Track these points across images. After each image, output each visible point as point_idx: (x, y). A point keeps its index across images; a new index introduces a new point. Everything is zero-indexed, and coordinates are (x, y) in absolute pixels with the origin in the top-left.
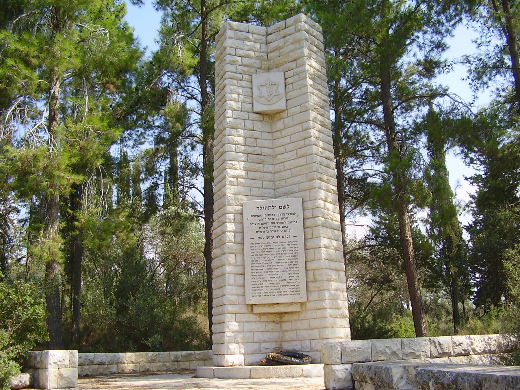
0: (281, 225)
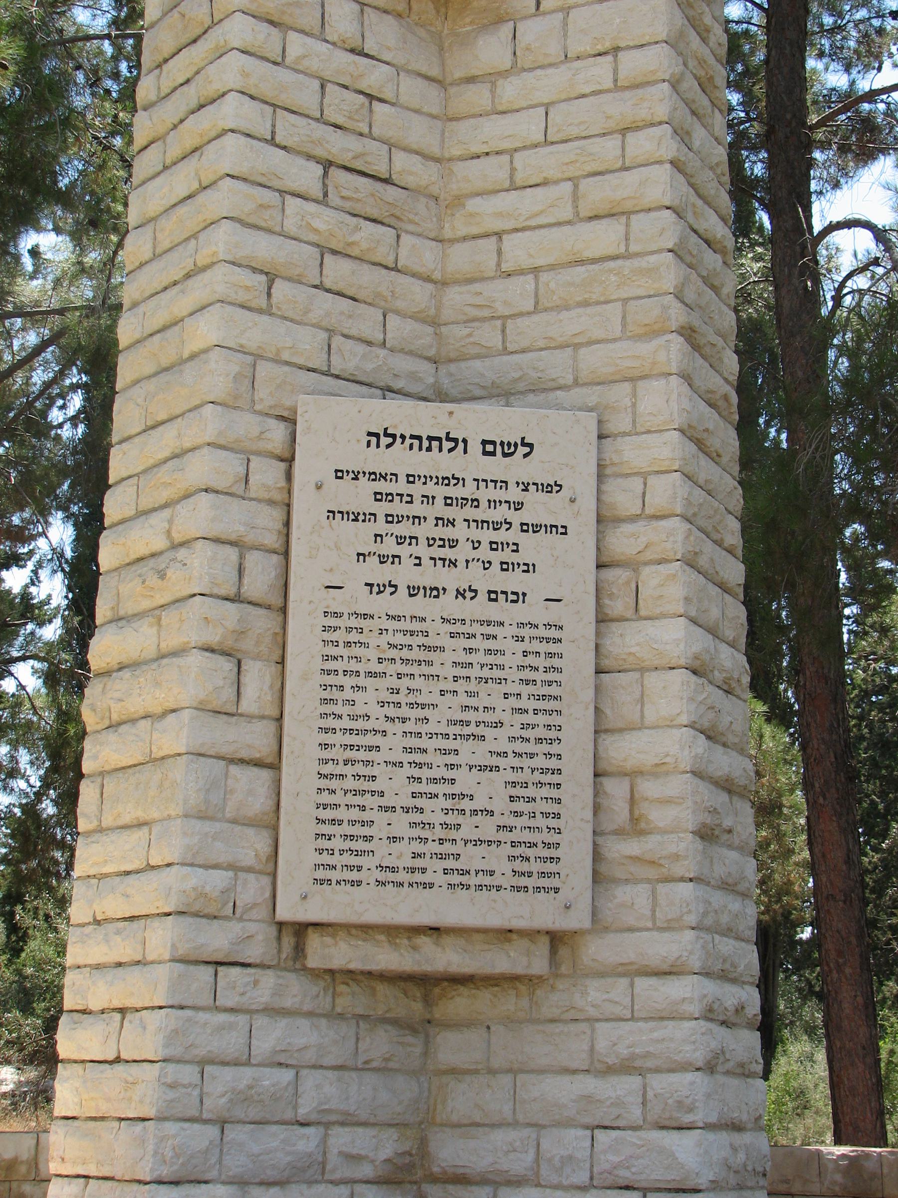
0: (487, 535)
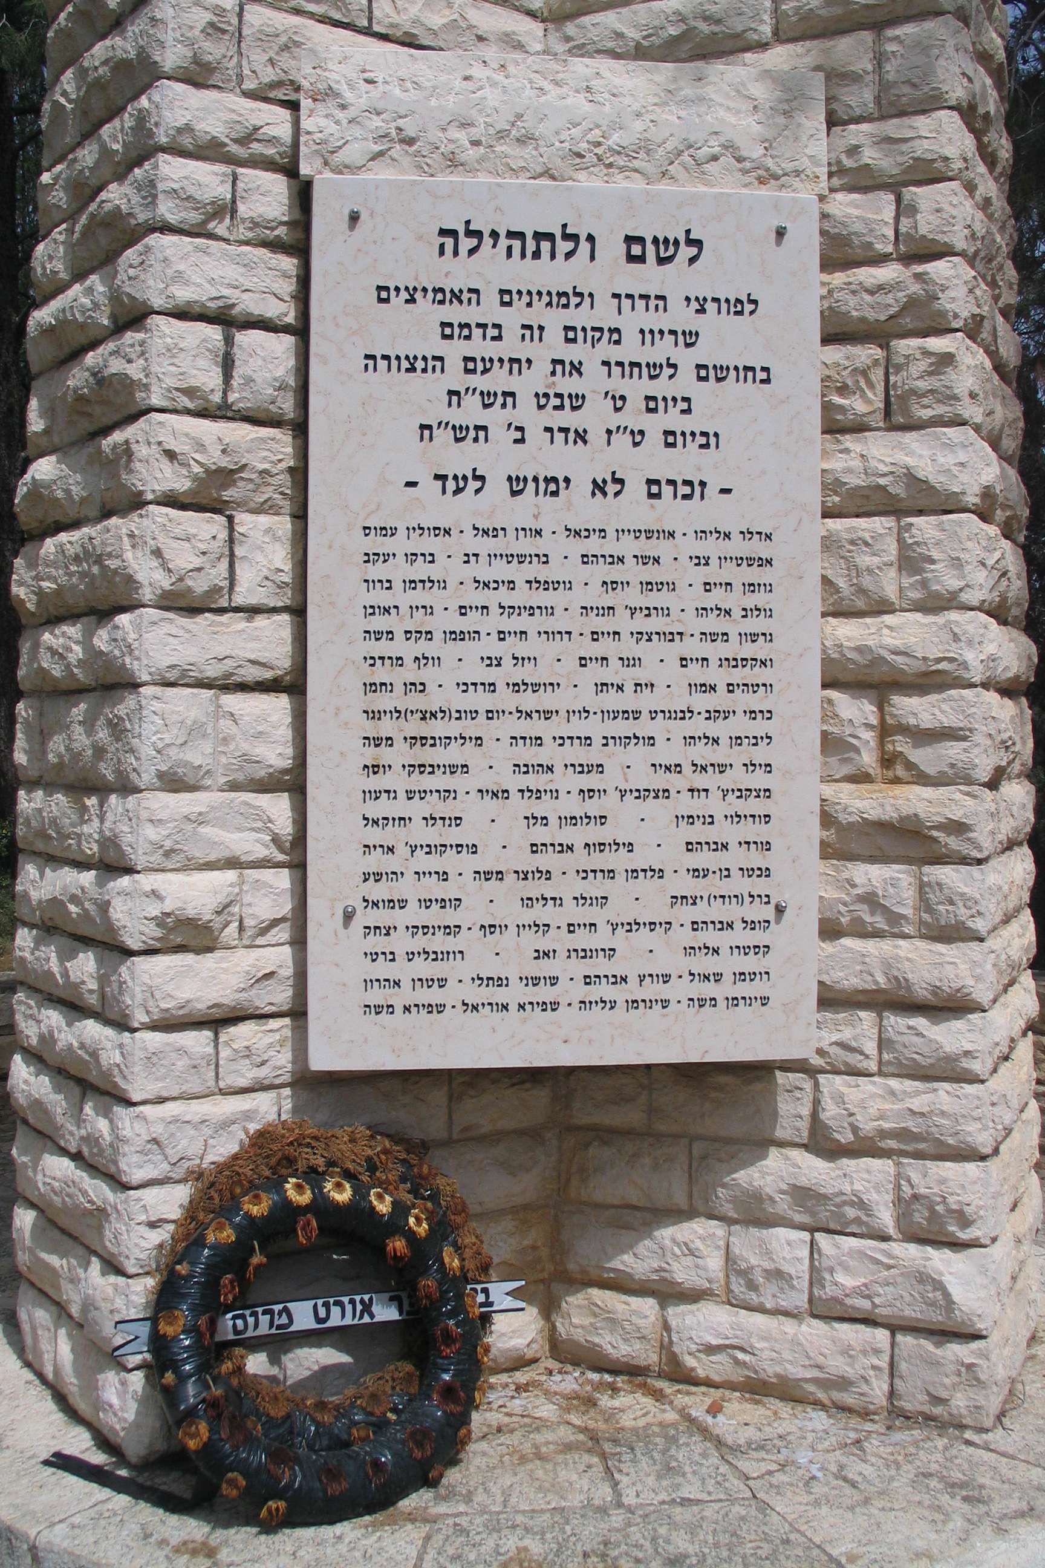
0: (636, 388)
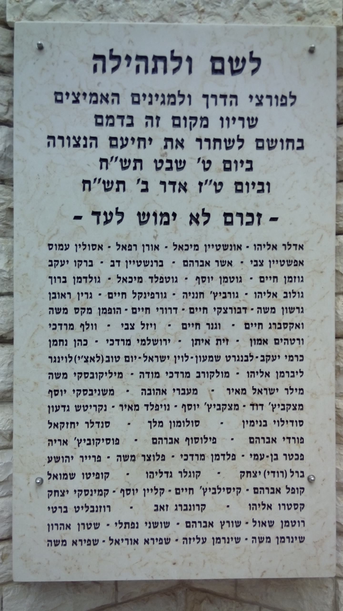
0: (218, 156)
